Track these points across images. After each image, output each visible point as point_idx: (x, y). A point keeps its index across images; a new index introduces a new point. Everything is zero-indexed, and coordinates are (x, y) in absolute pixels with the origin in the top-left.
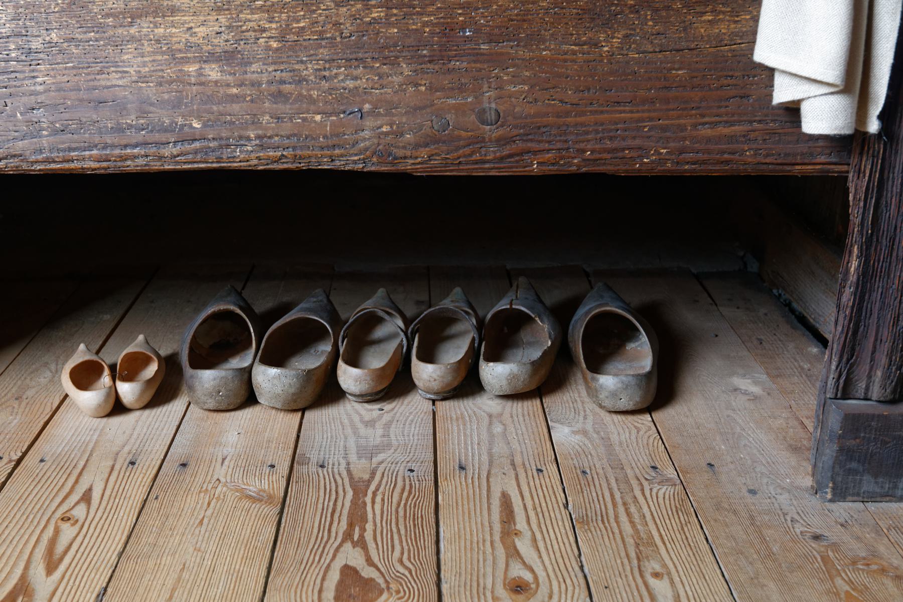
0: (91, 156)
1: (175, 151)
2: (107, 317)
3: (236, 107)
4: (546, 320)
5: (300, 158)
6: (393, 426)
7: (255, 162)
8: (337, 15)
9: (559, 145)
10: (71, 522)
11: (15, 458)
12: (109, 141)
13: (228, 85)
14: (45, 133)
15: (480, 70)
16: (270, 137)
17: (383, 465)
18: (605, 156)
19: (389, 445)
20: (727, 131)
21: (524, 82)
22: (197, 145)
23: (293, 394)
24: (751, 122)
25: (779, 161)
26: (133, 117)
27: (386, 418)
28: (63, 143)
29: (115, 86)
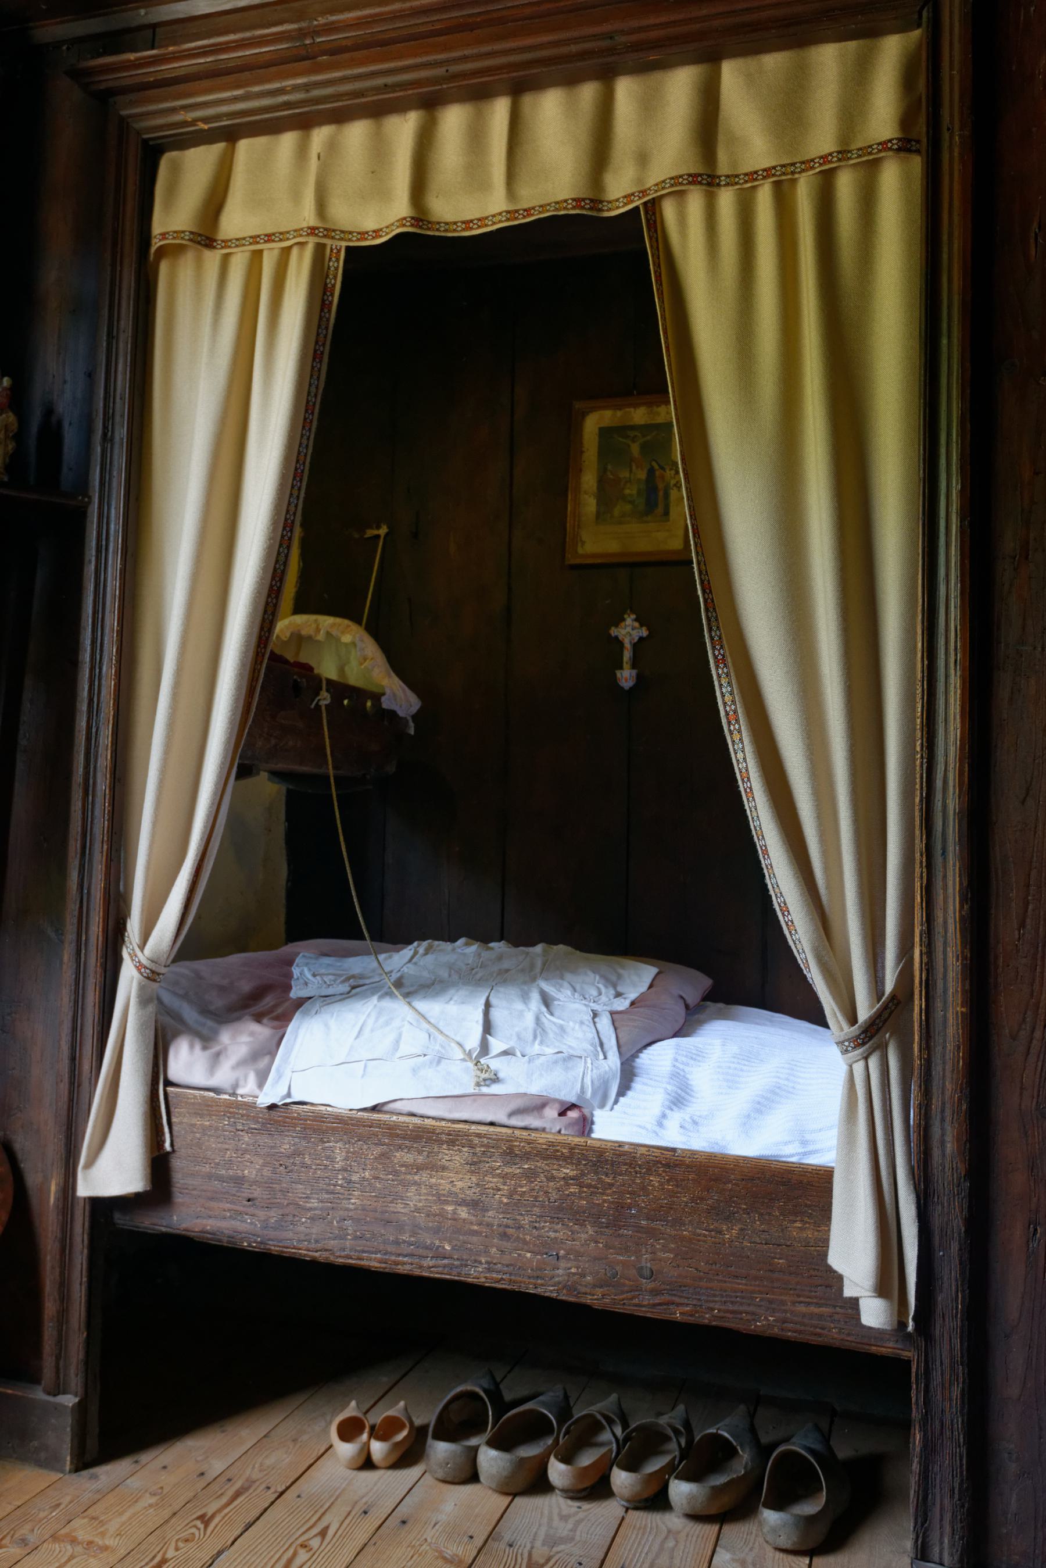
0: (375, 1258)
1: (431, 1263)
2: (385, 1379)
3: (475, 1239)
4: (748, 1450)
5: (514, 1282)
6: (583, 1524)
7: (483, 1280)
8: (547, 1186)
9: (695, 1302)
10: (307, 1549)
11: (280, 1490)
12: (389, 1250)
13: (471, 1223)
14: (349, 1237)
15: (640, 1238)
16: (495, 1264)
17: (560, 1555)
18: (728, 1315)
19: (572, 1539)
20: (816, 1310)
21: (670, 1251)
22: (446, 1261)
23: (506, 1477)
24: (835, 1307)
25: (858, 1341)
26: (407, 1235)
27: (581, 1515)
28: (360, 1246)
29: (399, 1212)
